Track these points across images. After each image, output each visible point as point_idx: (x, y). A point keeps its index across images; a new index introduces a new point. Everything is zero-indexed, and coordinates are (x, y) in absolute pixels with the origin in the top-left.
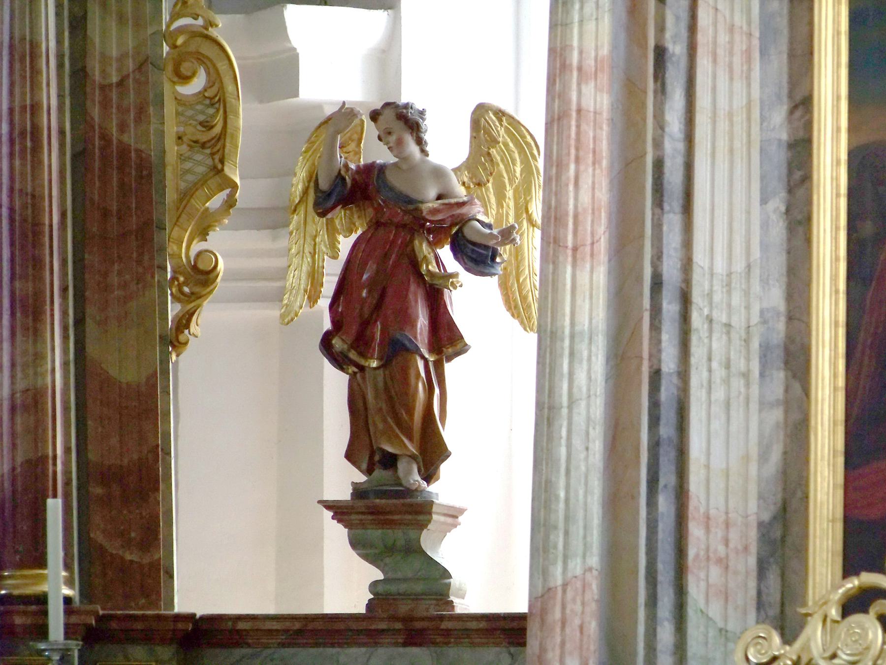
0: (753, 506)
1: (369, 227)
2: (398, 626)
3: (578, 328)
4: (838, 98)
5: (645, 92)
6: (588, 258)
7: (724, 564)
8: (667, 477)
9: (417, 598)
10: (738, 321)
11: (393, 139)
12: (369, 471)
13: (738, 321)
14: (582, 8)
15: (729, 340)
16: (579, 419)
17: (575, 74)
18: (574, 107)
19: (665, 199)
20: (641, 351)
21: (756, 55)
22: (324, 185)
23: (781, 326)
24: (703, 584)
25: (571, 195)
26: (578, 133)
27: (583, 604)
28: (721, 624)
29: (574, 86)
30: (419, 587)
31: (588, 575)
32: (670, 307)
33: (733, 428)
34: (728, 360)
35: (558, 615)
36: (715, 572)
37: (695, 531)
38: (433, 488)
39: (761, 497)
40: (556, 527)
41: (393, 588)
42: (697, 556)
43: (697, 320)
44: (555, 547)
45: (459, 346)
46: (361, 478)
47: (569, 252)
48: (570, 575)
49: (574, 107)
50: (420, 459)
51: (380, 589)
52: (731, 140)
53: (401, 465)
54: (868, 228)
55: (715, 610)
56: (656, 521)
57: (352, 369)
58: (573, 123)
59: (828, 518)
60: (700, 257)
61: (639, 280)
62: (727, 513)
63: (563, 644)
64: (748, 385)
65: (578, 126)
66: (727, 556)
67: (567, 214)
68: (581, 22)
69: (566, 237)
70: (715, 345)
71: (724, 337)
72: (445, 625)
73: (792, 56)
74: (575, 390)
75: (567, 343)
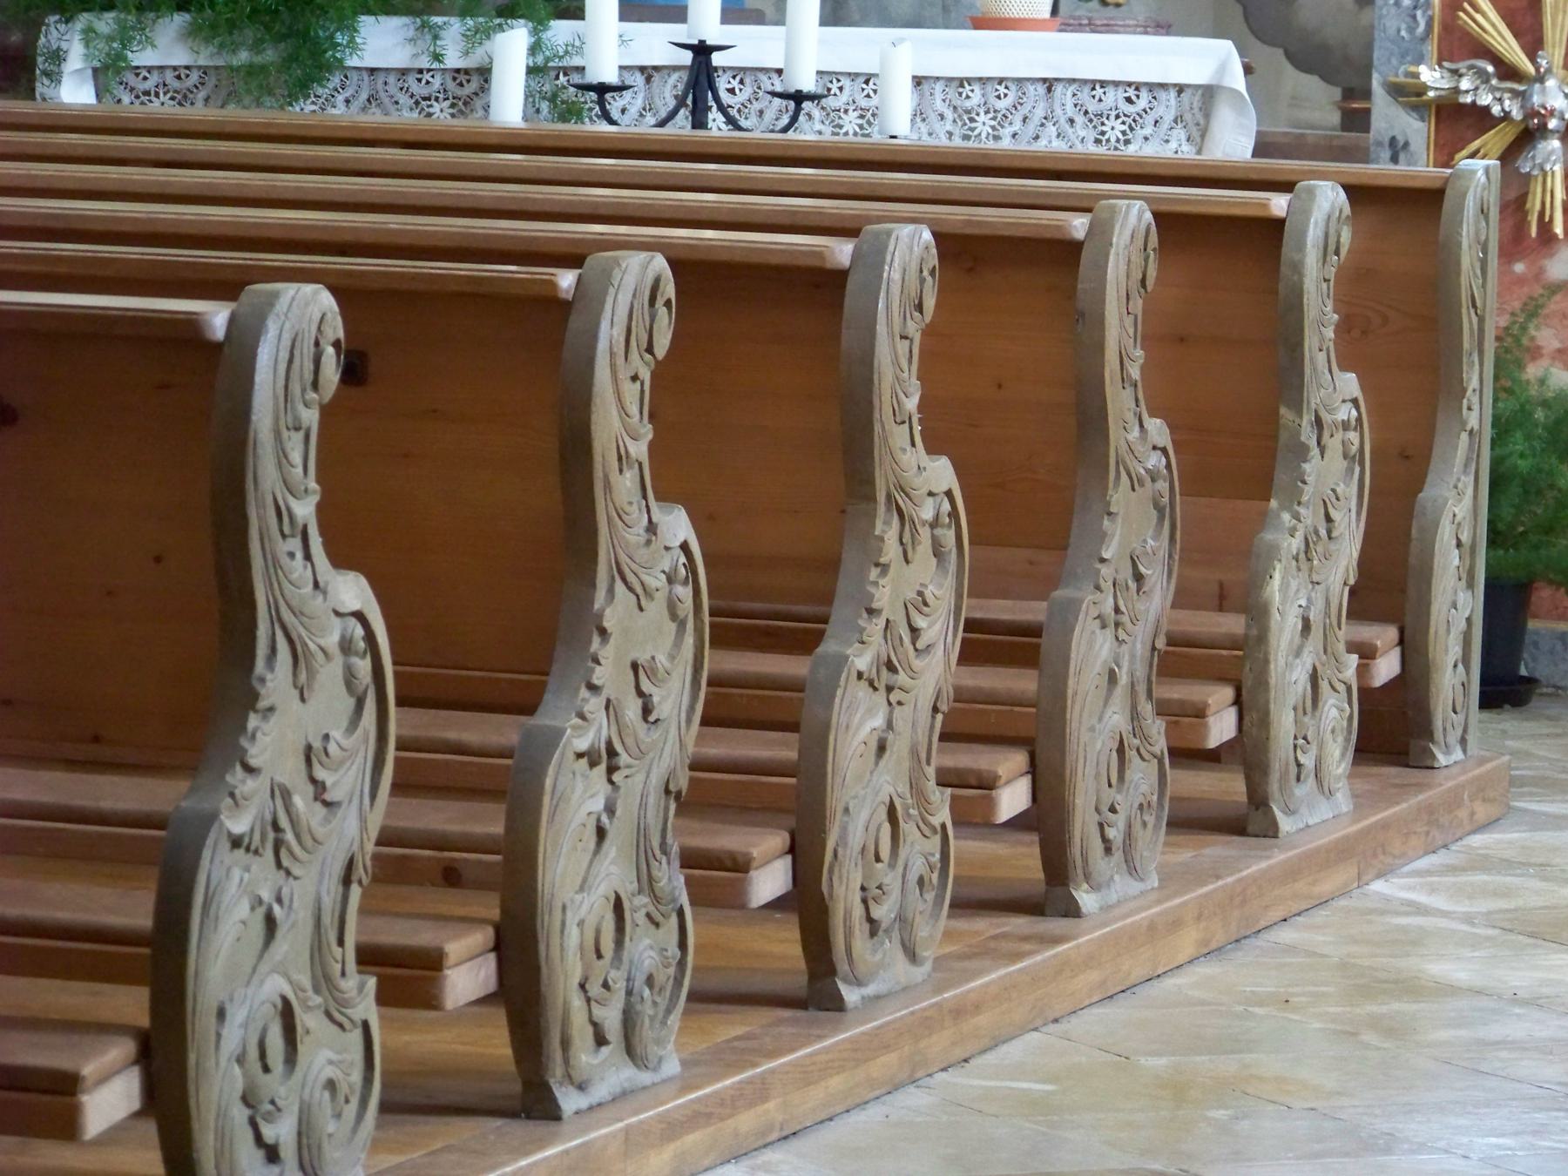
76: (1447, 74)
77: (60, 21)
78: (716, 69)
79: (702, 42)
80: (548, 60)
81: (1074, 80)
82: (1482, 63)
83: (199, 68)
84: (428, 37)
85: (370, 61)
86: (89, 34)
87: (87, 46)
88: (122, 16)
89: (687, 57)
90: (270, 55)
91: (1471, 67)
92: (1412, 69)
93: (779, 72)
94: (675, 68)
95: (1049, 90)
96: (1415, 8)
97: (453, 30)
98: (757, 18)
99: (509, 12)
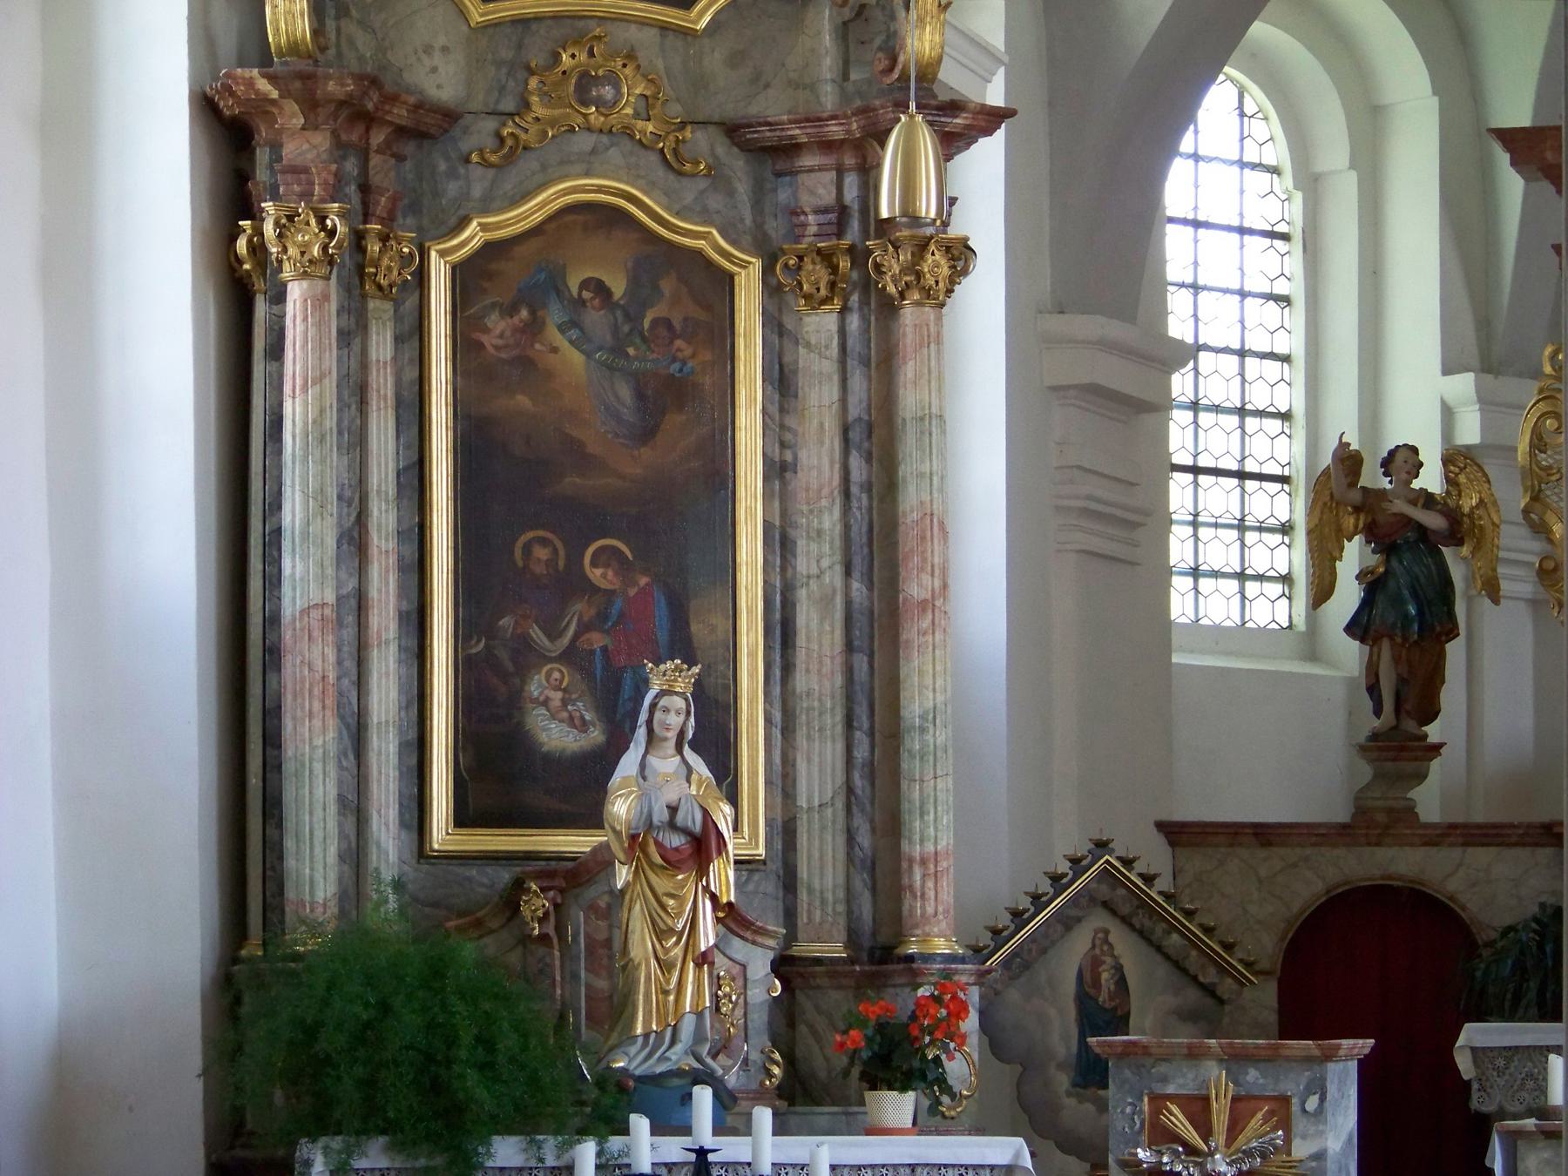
59: (1394, 760)
76: (1154, 1153)
77: (308, 1142)
78: (710, 1163)
79: (701, 1147)
80: (608, 1160)
81: (928, 1165)
82: (1175, 1146)
83: (395, 1169)
84: (535, 1148)
85: (499, 1163)
86: (326, 1151)
87: (325, 1157)
88: (347, 1138)
89: (692, 1157)
90: (439, 1161)
91: (1168, 1149)
92: (1133, 1151)
93: (749, 1164)
94: (685, 1164)
95: (913, 1171)
96: (1134, 1114)
97: (550, 1144)
98: (734, 1132)
99: (583, 1132)
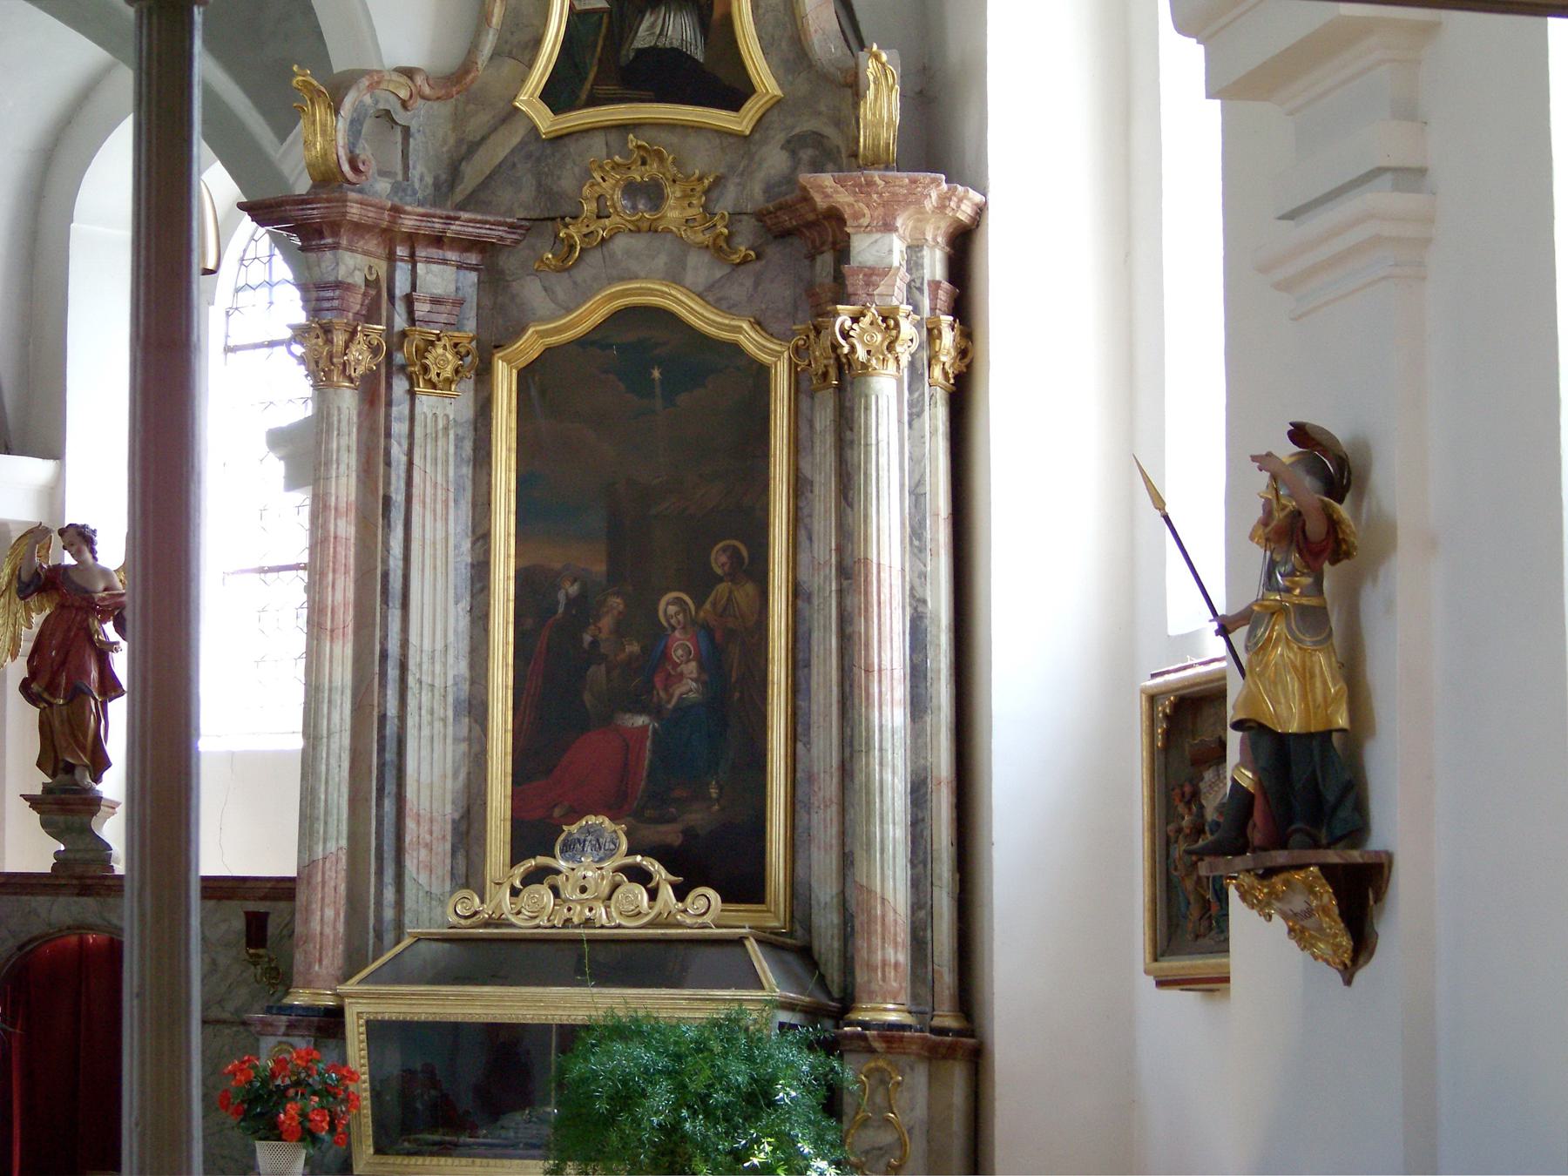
0: (449, 809)
1: (56, 609)
2: (75, 882)
3: (334, 685)
4: (509, 535)
5: (377, 527)
6: (341, 637)
7: (429, 847)
8: (390, 787)
9: (87, 863)
10: (438, 683)
11: (74, 549)
12: (53, 776)
13: (438, 683)
14: (338, 468)
15: (433, 695)
16: (335, 747)
17: (333, 512)
18: (332, 534)
19: (390, 599)
20: (373, 700)
21: (452, 504)
22: (25, 577)
23: (466, 687)
24: (415, 861)
25: (330, 594)
26: (335, 552)
27: (336, 872)
28: (427, 889)
29: (332, 521)
30: (88, 856)
31: (340, 852)
32: (393, 673)
33: (436, 756)
34: (432, 709)
35: (319, 879)
36: (423, 853)
37: (410, 824)
38: (99, 787)
39: (453, 803)
40: (318, 819)
41: (70, 856)
42: (412, 840)
43: (411, 681)
44: (318, 833)
45: (120, 691)
46: (49, 780)
47: (328, 633)
48: (328, 852)
49: (332, 534)
50: (91, 768)
51: (61, 856)
52: (435, 558)
53: (78, 773)
54: (529, 623)
55: (423, 878)
56: (383, 817)
57: (43, 705)
58: (332, 546)
60: (414, 638)
61: (373, 653)
62: (431, 813)
63: (323, 898)
64: (445, 726)
65: (335, 548)
66: (431, 841)
67: (327, 607)
68: (337, 477)
69: (326, 622)
70: (424, 699)
71: (430, 694)
72: (108, 882)
73: (474, 505)
74: (332, 726)
75: (326, 695)
